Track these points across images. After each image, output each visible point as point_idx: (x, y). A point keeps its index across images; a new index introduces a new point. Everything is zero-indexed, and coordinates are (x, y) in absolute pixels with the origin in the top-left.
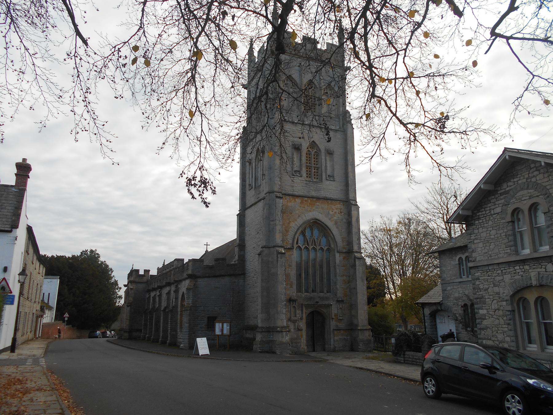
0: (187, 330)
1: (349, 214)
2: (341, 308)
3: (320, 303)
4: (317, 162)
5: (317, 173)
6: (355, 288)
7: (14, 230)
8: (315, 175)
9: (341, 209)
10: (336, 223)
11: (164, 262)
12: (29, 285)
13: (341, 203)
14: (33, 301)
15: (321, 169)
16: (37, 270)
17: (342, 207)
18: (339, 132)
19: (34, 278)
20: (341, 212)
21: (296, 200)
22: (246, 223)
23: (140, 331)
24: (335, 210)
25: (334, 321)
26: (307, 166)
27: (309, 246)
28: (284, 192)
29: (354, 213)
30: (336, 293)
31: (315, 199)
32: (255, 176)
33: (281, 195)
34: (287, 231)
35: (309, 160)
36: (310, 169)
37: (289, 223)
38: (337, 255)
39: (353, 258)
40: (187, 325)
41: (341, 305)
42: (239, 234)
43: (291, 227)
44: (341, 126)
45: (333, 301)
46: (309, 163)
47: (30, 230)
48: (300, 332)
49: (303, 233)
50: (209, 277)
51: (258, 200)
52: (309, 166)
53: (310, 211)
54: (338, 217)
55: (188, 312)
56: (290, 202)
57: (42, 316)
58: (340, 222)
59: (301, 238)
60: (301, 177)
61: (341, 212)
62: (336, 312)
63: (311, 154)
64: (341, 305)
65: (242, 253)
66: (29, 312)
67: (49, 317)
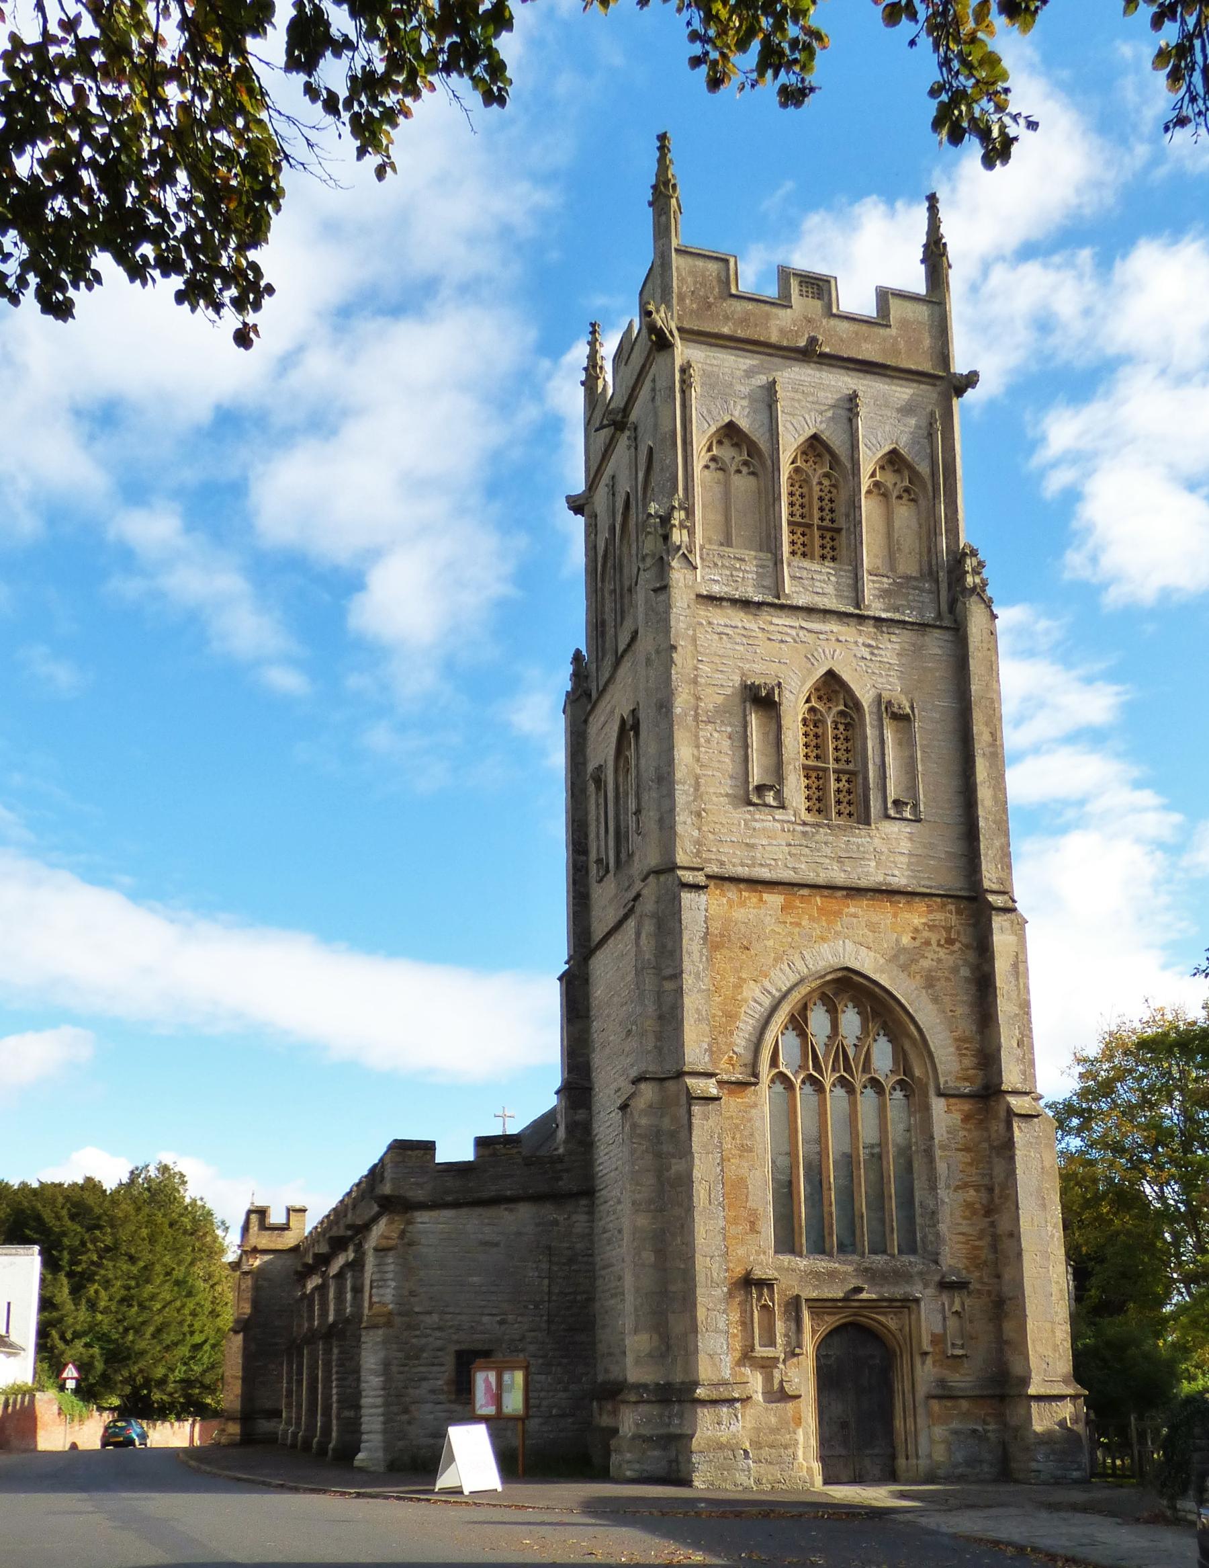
0: (379, 1401)
1: (983, 949)
2: (956, 1312)
4: (847, 751)
6: (1015, 1235)
8: (839, 802)
9: (948, 929)
10: (930, 982)
15: (866, 778)
17: (954, 919)
18: (937, 633)
22: (594, 1003)
23: (277, 1414)
24: (926, 934)
25: (929, 1360)
26: (805, 767)
27: (821, 1074)
28: (713, 869)
29: (1001, 939)
30: (938, 1254)
31: (840, 894)
34: (731, 1016)
35: (817, 747)
37: (738, 987)
38: (938, 1106)
39: (1003, 1114)
41: (957, 1301)
42: (569, 1046)
43: (745, 1000)
44: (944, 607)
45: (926, 1286)
48: (790, 1405)
49: (798, 1023)
50: (456, 1205)
51: (626, 910)
52: (815, 769)
53: (823, 939)
54: (939, 960)
55: (380, 1332)
56: (742, 904)
58: (948, 979)
59: (790, 1045)
60: (783, 807)
61: (950, 941)
62: (938, 1330)
63: (824, 722)
64: (957, 1301)
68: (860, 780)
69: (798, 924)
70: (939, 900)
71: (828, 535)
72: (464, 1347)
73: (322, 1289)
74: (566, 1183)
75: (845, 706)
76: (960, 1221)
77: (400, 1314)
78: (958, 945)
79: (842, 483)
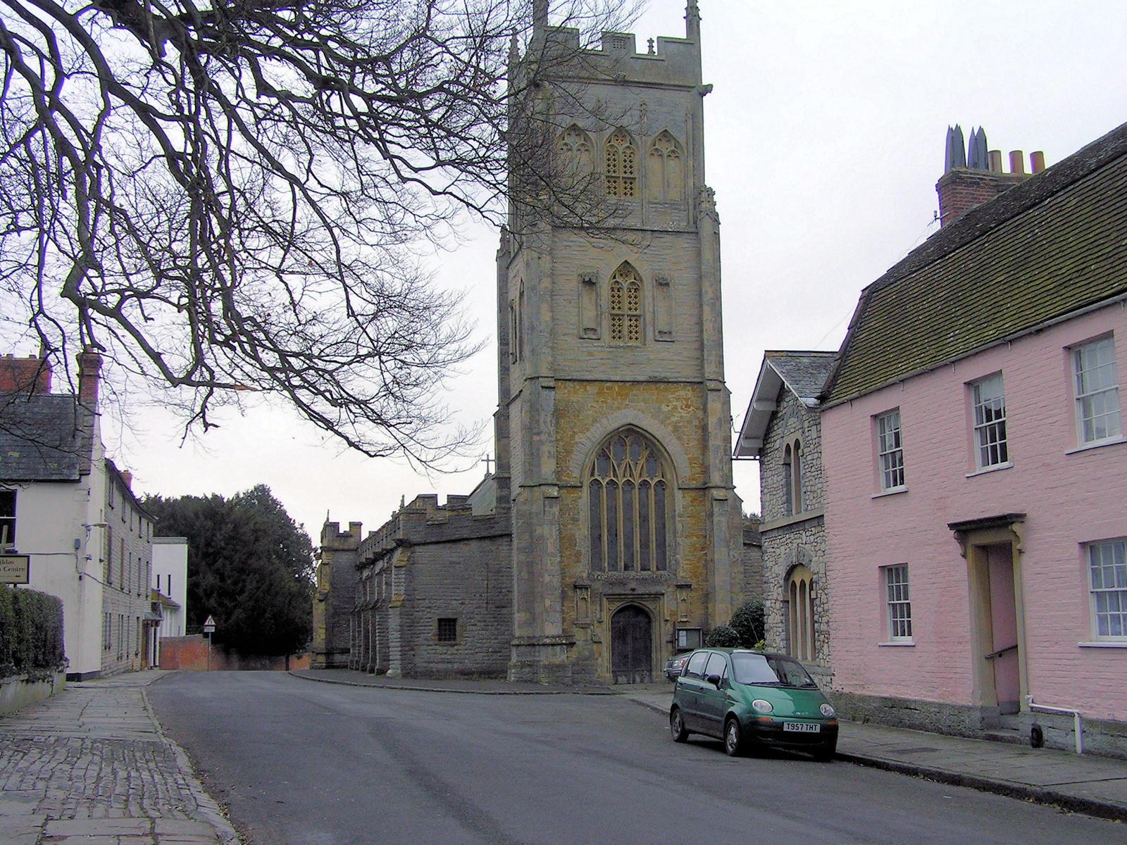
3: (640, 590)
5: (636, 326)
7: (84, 478)
11: (403, 501)
12: (122, 563)
13: (690, 388)
14: (135, 592)
16: (136, 531)
17: (690, 394)
19: (130, 548)
20: (688, 406)
21: (588, 388)
32: (521, 337)
33: (552, 384)
36: (619, 320)
37: (572, 437)
40: (397, 635)
46: (619, 308)
47: (110, 466)
53: (618, 408)
54: (681, 417)
56: (575, 392)
57: (157, 623)
65: (505, 492)
66: (127, 614)
67: (173, 626)
68: (642, 320)
69: (606, 402)
70: (682, 384)
71: (629, 181)
72: (442, 617)
73: (369, 578)
74: (498, 530)
75: (635, 279)
76: (687, 553)
77: (408, 600)
78: (692, 408)
79: (636, 152)
